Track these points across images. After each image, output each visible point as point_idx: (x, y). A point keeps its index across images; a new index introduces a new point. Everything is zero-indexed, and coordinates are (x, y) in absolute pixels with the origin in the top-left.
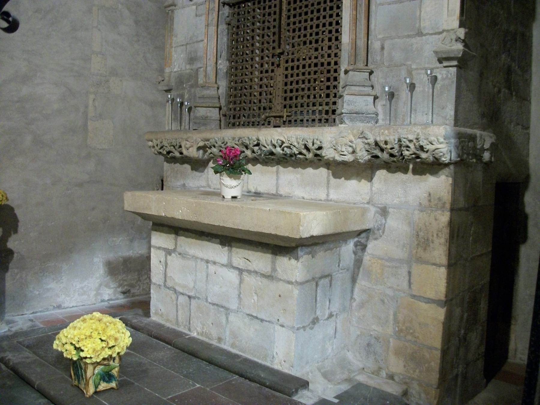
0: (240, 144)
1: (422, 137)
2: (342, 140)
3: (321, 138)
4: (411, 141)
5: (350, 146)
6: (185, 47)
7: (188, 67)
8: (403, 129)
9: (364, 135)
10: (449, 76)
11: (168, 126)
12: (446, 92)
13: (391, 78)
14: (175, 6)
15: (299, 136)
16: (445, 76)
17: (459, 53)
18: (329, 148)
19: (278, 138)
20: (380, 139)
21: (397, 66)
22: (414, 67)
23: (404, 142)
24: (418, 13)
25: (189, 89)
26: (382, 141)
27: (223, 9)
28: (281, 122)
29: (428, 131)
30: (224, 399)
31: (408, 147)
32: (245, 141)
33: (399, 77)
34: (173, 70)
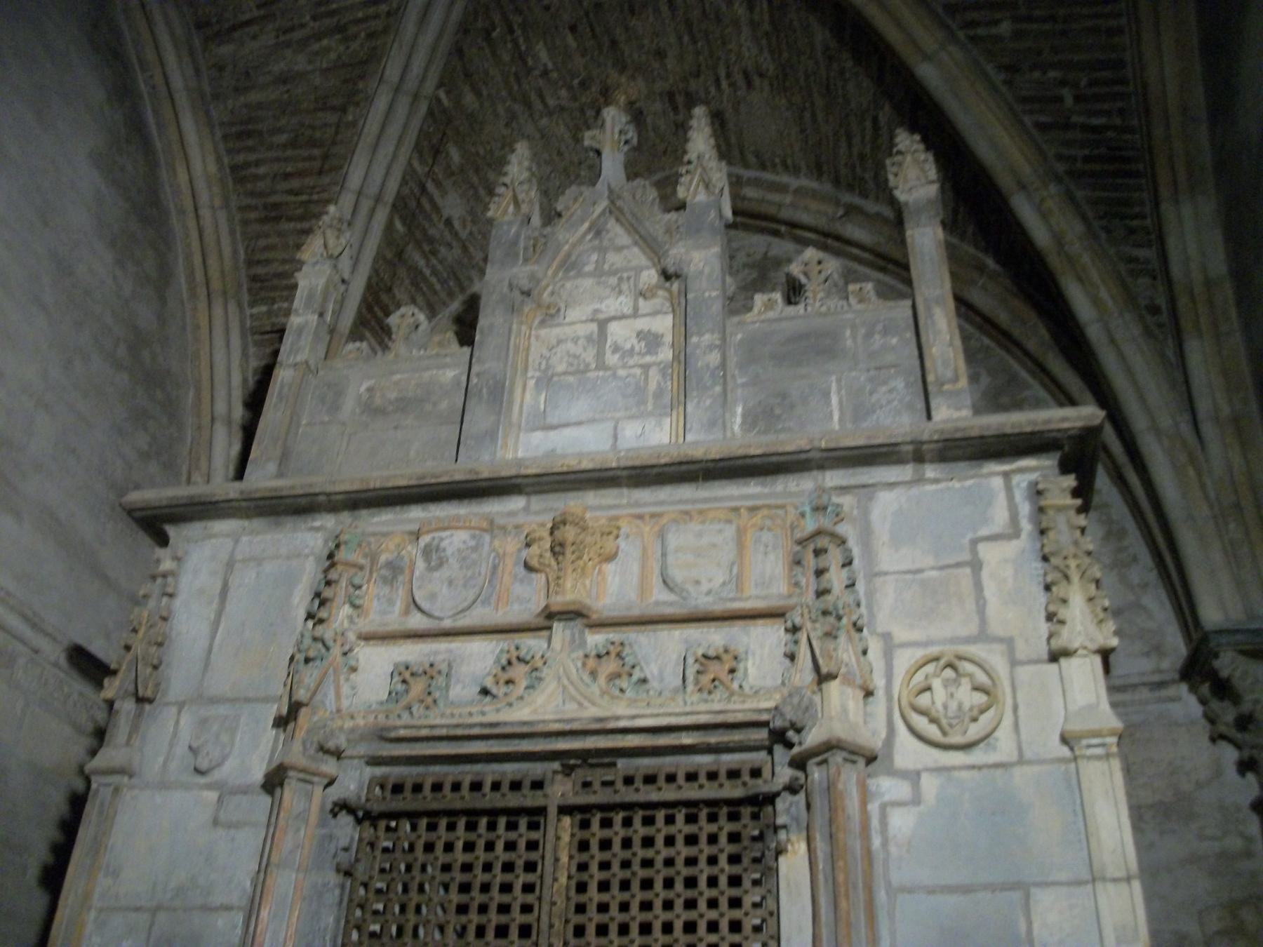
6: (145, 917)
11: (328, 50)
14: (131, 776)
24: (1023, 927)
30: (435, 718)
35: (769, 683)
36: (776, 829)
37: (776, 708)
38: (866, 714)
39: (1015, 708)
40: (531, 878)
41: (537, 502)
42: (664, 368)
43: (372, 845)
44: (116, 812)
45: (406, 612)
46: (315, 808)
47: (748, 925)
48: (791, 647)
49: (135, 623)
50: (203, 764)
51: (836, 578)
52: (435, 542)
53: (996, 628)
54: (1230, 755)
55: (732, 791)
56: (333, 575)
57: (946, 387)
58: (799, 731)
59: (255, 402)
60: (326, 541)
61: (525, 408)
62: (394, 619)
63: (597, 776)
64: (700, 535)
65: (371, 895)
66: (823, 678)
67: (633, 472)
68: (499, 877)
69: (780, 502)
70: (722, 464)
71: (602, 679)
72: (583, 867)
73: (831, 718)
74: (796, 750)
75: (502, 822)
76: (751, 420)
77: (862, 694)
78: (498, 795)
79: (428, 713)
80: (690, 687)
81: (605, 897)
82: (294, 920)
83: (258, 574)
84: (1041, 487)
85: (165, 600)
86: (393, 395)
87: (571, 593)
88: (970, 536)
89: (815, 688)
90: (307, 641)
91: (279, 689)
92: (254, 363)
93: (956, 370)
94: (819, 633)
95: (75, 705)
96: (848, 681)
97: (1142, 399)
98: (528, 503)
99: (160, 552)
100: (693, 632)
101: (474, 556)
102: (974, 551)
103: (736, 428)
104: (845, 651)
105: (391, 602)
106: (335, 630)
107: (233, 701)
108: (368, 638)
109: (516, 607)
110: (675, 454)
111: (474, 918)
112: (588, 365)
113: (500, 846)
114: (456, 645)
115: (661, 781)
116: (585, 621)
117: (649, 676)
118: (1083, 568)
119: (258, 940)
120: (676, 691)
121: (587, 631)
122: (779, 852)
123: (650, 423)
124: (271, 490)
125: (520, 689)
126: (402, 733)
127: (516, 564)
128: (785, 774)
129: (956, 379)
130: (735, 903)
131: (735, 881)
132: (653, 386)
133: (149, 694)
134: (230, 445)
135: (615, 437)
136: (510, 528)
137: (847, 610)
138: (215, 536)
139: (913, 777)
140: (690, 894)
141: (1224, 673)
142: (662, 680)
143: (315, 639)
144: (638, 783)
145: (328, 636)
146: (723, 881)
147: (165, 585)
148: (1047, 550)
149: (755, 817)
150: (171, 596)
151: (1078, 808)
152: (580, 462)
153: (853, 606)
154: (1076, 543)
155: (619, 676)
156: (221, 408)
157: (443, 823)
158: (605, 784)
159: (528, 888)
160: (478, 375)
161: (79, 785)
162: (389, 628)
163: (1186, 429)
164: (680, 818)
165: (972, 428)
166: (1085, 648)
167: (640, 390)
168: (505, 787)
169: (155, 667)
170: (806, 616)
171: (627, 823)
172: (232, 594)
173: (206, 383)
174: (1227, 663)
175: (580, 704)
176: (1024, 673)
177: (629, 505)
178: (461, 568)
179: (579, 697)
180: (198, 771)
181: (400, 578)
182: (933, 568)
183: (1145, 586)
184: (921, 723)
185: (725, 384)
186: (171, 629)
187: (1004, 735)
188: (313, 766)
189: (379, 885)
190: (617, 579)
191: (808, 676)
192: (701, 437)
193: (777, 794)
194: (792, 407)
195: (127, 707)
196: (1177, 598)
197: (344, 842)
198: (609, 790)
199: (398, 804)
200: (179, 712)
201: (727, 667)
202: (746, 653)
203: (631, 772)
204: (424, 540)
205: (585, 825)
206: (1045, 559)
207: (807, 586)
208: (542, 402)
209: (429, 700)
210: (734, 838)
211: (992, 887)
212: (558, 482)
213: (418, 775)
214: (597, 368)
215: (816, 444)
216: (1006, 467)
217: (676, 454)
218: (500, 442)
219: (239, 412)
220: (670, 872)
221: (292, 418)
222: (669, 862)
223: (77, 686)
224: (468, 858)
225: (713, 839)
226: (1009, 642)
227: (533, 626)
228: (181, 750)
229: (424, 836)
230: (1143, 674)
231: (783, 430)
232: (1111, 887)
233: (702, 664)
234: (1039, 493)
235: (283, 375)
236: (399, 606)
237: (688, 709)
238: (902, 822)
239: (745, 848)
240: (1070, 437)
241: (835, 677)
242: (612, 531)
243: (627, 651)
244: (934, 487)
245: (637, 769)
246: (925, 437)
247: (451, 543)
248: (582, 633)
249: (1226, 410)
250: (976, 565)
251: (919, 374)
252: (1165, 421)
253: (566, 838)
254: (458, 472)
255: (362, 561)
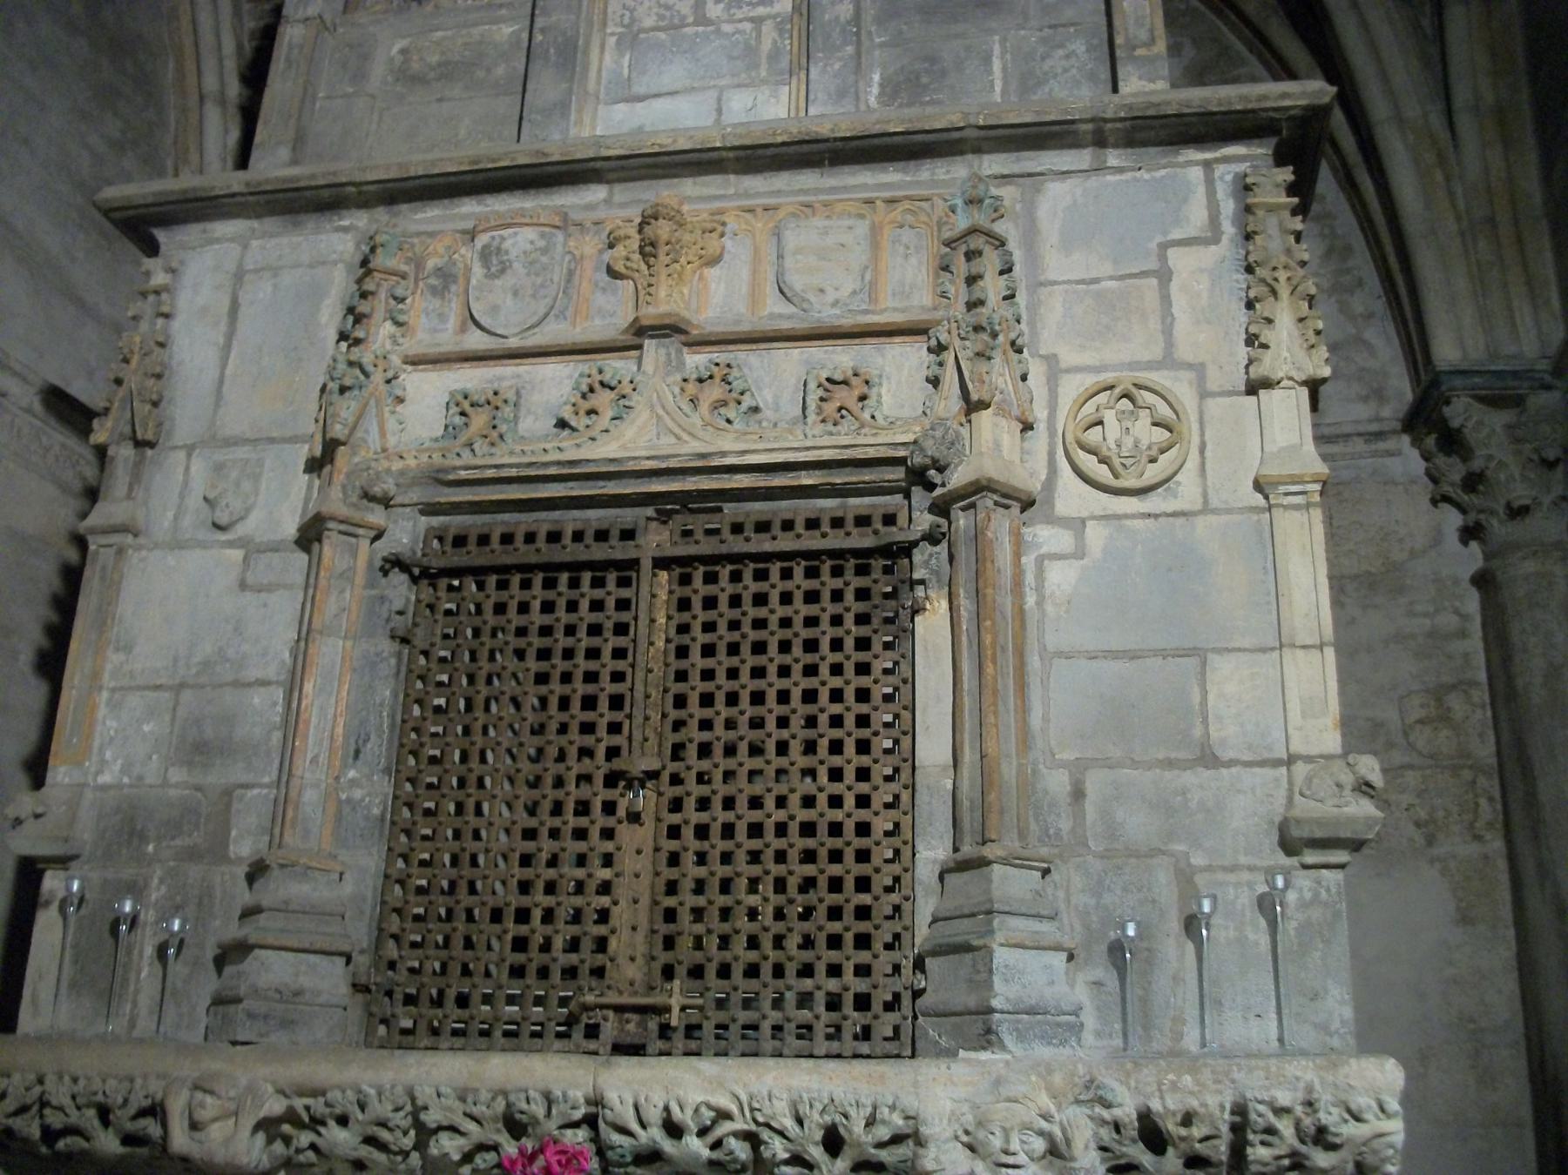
0: (495, 1119)
1: (1324, 1097)
2: (1007, 1109)
3: (910, 1102)
4: (1280, 1111)
5: (1041, 1133)
7: (177, 775)
8: (1251, 1070)
9: (1100, 1092)
10: (1324, 894)
12: (1321, 946)
13: (1118, 892)
14: (136, 535)
15: (809, 1090)
16: (1308, 895)
17: (1370, 828)
18: (947, 1141)
19: (700, 1099)
20: (1166, 1106)
21: (1136, 854)
22: (1198, 860)
23: (1260, 1115)
24: (1196, 698)
25: (172, 864)
26: (1174, 1114)
27: (384, 580)
28: (646, 1029)
29: (1347, 1076)
31: (1270, 1131)
32: (524, 1106)
33: (1149, 889)
34: (90, 780)
35: (906, 413)
36: (913, 584)
37: (915, 442)
38: (1023, 451)
39: (1202, 451)
40: (622, 641)
41: (622, 192)
42: (782, 22)
43: (431, 607)
44: (122, 577)
45: (463, 329)
46: (362, 562)
47: (878, 692)
48: (935, 370)
49: (126, 351)
50: (223, 519)
51: (992, 287)
52: (495, 243)
53: (1184, 352)
54: (1453, 520)
55: (861, 540)
56: (369, 285)
57: (1140, 52)
58: (941, 470)
59: (255, 74)
60: (358, 245)
61: (604, 74)
62: (448, 338)
63: (699, 523)
64: (825, 232)
65: (433, 666)
66: (972, 406)
67: (741, 153)
68: (585, 641)
69: (925, 192)
70: (854, 144)
71: (704, 407)
72: (683, 629)
73: (981, 454)
74: (938, 491)
75: (587, 577)
76: (890, 91)
77: (1021, 426)
78: (581, 546)
79: (493, 450)
80: (812, 417)
81: (710, 663)
82: (344, 694)
83: (275, 286)
84: (1249, 180)
85: (160, 321)
86: (434, 59)
87: (667, 302)
88: (1159, 239)
89: (964, 420)
90: (342, 366)
91: (310, 427)
92: (250, 24)
93: (1152, 31)
94: (970, 353)
95: (57, 460)
96: (1003, 412)
97: (1384, 77)
98: (611, 193)
99: (149, 263)
100: (817, 352)
101: (544, 259)
102: (1163, 258)
103: (873, 101)
104: (999, 376)
105: (442, 317)
106: (374, 352)
107: (256, 441)
108: (415, 361)
109: (597, 322)
110: (795, 131)
111: (556, 688)
112: (684, 18)
113: (584, 605)
114: (524, 369)
115: (776, 529)
116: (683, 338)
117: (761, 405)
118: (1294, 282)
119: (303, 716)
120: (794, 422)
121: (685, 349)
122: (916, 611)
123: (764, 92)
124: (285, 180)
125: (604, 420)
126: (463, 474)
127: (597, 269)
128: (925, 521)
129: (1152, 41)
130: (863, 669)
131: (863, 644)
132: (766, 45)
133: (150, 436)
134: (226, 131)
135: (719, 111)
136: (588, 224)
137: (1004, 325)
138: (218, 240)
139: (1077, 525)
140: (810, 658)
141: (1455, 423)
142: (777, 409)
143: (351, 364)
144: (749, 531)
145: (367, 359)
146: (849, 643)
147: (159, 303)
148: (1251, 259)
149: (888, 570)
150: (167, 316)
151: (1270, 565)
152: (675, 141)
153: (1013, 322)
154: (1288, 252)
155: (724, 403)
156: (210, 83)
157: (516, 580)
158: (710, 532)
159: (619, 654)
160: (542, 31)
161: (72, 555)
162: (443, 349)
163: (1437, 121)
164: (799, 572)
165: (1168, 103)
166: (1291, 379)
167: (750, 52)
168: (589, 538)
169: (155, 404)
170: (955, 332)
171: (736, 577)
172: (245, 312)
173: (189, 50)
174: (1460, 411)
175: (679, 438)
176: (1215, 406)
177: (737, 195)
178: (528, 274)
179: (677, 430)
180: (217, 527)
181: (453, 288)
182: (1111, 278)
183: (1370, 316)
184: (1089, 462)
185: (859, 43)
186: (170, 357)
187: (1187, 479)
188: (356, 516)
189: (443, 653)
190: (723, 285)
191: (955, 404)
192: (829, 110)
193: (915, 544)
194: (944, 73)
195: (123, 453)
196: (1405, 323)
197: (398, 604)
198: (714, 539)
199: (458, 559)
200: (189, 456)
201: (857, 393)
202: (880, 376)
203: (740, 519)
204: (482, 240)
205: (685, 580)
206: (1249, 270)
207: (956, 297)
208: (626, 64)
209: (495, 434)
210: (863, 594)
211: (1163, 654)
212: (649, 166)
213: (484, 525)
214: (696, 23)
215: (972, 121)
216: (1208, 155)
217: (795, 131)
218: (573, 117)
219: (234, 89)
220: (787, 634)
221: (305, 89)
222: (786, 623)
223: (58, 437)
224: (547, 619)
225: (837, 596)
226: (1199, 369)
227: (619, 344)
228: (194, 501)
229: (495, 596)
230: (1357, 422)
231: (932, 102)
232: (1300, 653)
233: (827, 390)
234: (1247, 188)
235: (291, 35)
236: (452, 323)
237: (809, 443)
238: (1061, 577)
239: (876, 607)
240: (1291, 118)
241: (987, 406)
242: (716, 227)
243: (735, 373)
244: (1118, 177)
245: (748, 515)
246: (1109, 115)
247: (514, 245)
248: (679, 352)
249: (1489, 98)
250: (1164, 275)
251: (1105, 36)
252: (1412, 110)
253: (663, 595)
254: (521, 155)
255: (404, 268)
